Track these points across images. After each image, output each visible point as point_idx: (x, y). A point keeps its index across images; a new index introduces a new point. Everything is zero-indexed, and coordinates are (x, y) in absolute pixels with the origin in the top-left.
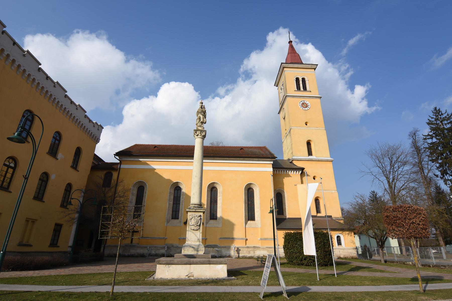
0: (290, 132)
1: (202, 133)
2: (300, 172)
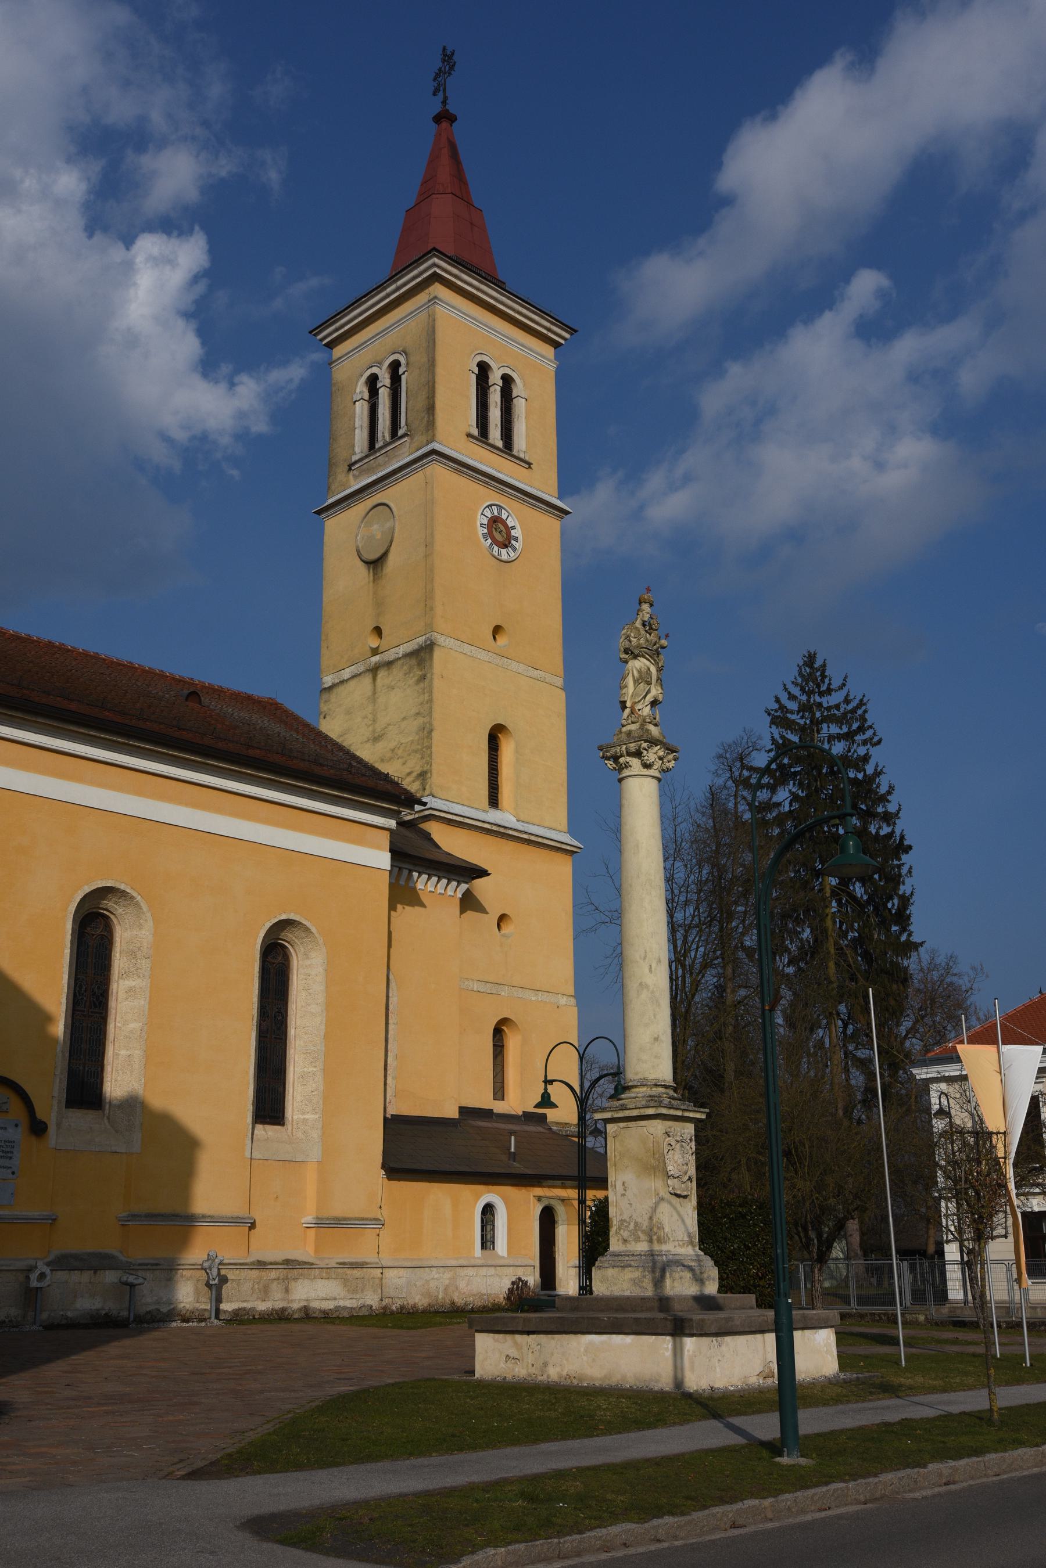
0: (423, 654)
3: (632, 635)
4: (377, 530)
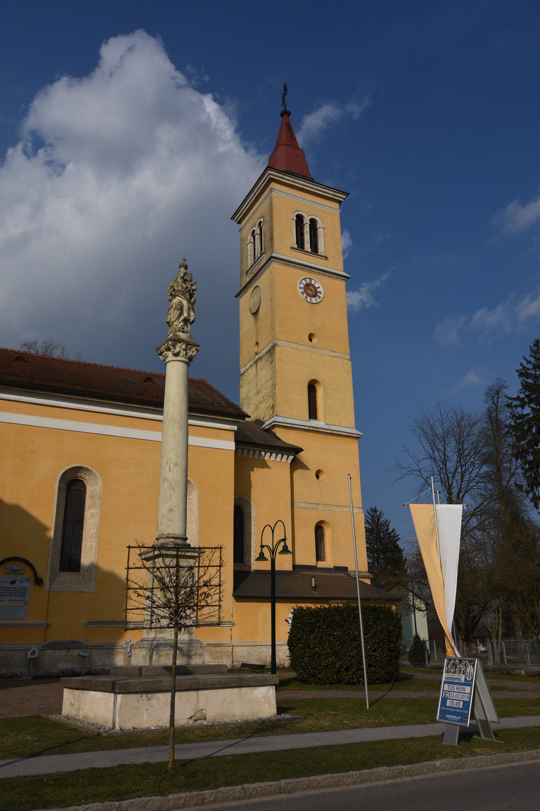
0: (271, 351)
1: (190, 349)
2: (291, 457)
3: (175, 285)
4: (256, 299)
